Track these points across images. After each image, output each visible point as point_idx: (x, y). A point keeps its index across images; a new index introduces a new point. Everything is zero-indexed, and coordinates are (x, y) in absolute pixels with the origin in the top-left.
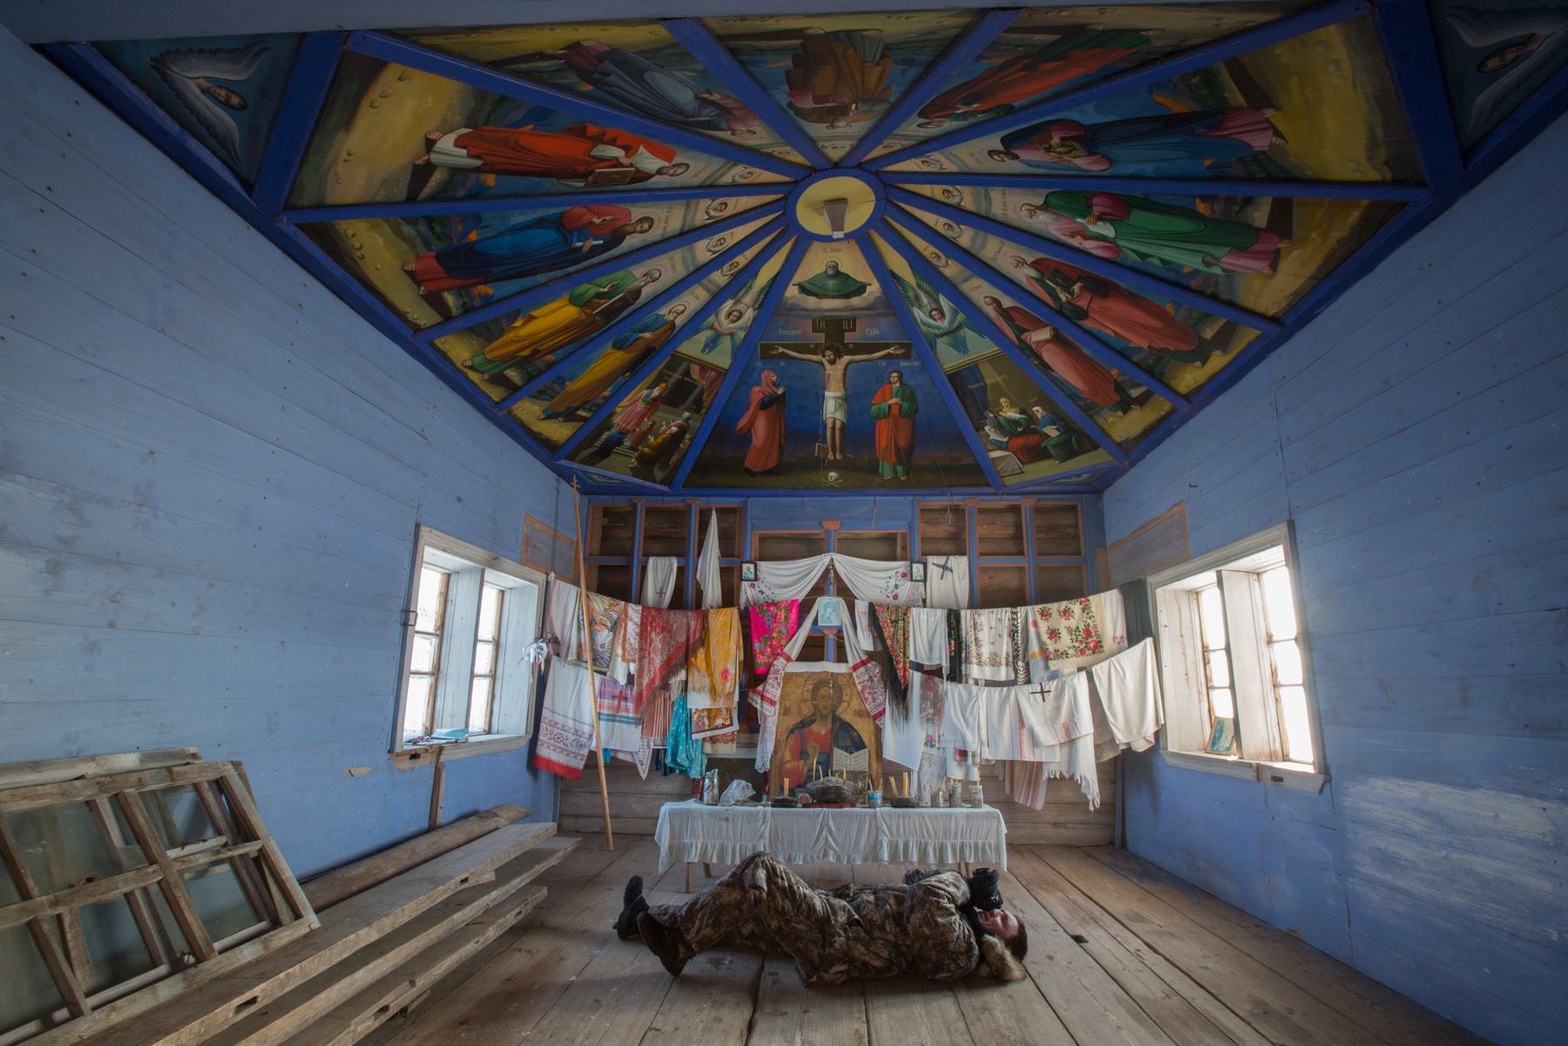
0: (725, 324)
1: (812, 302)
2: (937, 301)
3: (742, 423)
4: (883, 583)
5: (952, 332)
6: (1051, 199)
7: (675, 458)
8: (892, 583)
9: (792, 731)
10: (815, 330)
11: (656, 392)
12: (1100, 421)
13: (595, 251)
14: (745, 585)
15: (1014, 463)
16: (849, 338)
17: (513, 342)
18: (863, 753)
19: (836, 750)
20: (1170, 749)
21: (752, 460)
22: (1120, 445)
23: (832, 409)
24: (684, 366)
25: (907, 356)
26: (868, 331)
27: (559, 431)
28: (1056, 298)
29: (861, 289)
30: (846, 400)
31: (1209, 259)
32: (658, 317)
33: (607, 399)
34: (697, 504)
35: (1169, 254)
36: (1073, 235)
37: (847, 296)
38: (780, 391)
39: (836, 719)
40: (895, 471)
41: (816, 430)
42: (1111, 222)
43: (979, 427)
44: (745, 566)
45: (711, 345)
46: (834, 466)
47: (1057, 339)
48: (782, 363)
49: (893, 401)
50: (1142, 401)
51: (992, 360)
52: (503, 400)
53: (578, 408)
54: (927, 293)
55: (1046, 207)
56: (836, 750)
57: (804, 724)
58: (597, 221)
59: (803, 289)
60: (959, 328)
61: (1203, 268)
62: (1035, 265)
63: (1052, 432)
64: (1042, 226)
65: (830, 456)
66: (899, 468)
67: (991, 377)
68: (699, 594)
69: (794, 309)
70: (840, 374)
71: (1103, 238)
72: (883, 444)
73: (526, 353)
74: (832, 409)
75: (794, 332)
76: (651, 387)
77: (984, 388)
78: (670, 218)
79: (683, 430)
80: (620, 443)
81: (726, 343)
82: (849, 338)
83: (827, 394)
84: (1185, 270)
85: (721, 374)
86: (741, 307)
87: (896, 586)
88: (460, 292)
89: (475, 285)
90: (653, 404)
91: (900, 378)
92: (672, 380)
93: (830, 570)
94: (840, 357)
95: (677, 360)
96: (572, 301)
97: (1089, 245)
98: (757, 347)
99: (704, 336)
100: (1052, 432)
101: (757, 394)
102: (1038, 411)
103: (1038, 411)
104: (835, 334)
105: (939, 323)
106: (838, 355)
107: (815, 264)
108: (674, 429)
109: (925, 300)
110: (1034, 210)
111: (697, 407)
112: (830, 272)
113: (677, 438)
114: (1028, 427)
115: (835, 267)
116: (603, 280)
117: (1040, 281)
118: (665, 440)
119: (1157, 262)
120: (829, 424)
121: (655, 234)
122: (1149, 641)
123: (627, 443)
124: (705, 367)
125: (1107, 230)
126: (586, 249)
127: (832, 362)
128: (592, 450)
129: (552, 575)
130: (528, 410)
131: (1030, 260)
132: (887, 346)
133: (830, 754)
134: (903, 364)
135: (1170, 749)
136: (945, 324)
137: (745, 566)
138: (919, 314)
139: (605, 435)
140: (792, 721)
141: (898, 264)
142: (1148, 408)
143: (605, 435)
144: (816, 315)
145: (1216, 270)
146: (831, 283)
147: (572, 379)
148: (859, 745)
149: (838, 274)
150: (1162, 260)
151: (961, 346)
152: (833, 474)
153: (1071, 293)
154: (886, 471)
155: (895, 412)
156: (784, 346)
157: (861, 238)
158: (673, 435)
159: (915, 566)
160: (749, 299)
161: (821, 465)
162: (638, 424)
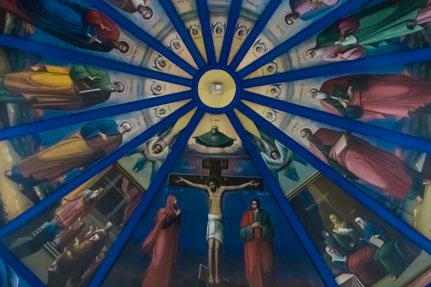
0: (151, 154)
1: (203, 149)
2: (274, 146)
3: (148, 241)
5: (286, 166)
6: (320, 39)
7: (88, 272)
10: (204, 167)
13: (95, 46)
16: (224, 173)
17: (25, 81)
24: (120, 176)
25: (261, 188)
26: (235, 169)
28: (339, 107)
29: (230, 142)
30: (225, 223)
31: (410, 23)
32: (115, 125)
35: (388, 34)
36: (336, 55)
37: (223, 146)
38: (178, 213)
42: (352, 34)
43: (321, 251)
45: (140, 166)
47: (353, 144)
48: (182, 190)
49: (255, 225)
51: (316, 181)
53: (37, 183)
54: (268, 142)
55: (318, 47)
58: (103, 28)
59: (198, 140)
60: (290, 161)
61: (410, 32)
62: (323, 90)
64: (319, 59)
65: (211, 280)
67: (320, 197)
69: (193, 152)
70: (218, 199)
71: (351, 47)
72: (251, 269)
73: (28, 96)
75: (191, 168)
76: (93, 188)
77: (316, 208)
78: (136, 54)
81: (148, 168)
82: (224, 173)
83: (211, 216)
84: (402, 39)
86: (162, 143)
88: (17, 20)
89: (27, 21)
90: (90, 203)
91: (258, 204)
92: (108, 187)
94: (219, 187)
95: (118, 170)
96: (73, 74)
97: (346, 56)
98: (167, 176)
99: (137, 157)
101: (162, 214)
104: (215, 165)
105: (277, 161)
106: (218, 185)
107: (206, 126)
109: (267, 146)
110: (312, 51)
112: (214, 132)
115: (216, 129)
116: (93, 70)
117: (328, 100)
119: (384, 44)
121: (127, 58)
124: (133, 184)
125: (351, 40)
126: (91, 41)
127: (214, 191)
128: (27, 239)
131: (319, 87)
132: (248, 180)
134: (260, 194)
136: (281, 161)
138: (265, 156)
141: (250, 126)
144: (205, 157)
145: (418, 28)
146: (214, 138)
149: (217, 133)
150: (388, 41)
151: (293, 175)
153: (347, 98)
155: (257, 235)
156: (184, 177)
157: (228, 111)
158: (95, 243)
160: (167, 139)
162: (71, 223)
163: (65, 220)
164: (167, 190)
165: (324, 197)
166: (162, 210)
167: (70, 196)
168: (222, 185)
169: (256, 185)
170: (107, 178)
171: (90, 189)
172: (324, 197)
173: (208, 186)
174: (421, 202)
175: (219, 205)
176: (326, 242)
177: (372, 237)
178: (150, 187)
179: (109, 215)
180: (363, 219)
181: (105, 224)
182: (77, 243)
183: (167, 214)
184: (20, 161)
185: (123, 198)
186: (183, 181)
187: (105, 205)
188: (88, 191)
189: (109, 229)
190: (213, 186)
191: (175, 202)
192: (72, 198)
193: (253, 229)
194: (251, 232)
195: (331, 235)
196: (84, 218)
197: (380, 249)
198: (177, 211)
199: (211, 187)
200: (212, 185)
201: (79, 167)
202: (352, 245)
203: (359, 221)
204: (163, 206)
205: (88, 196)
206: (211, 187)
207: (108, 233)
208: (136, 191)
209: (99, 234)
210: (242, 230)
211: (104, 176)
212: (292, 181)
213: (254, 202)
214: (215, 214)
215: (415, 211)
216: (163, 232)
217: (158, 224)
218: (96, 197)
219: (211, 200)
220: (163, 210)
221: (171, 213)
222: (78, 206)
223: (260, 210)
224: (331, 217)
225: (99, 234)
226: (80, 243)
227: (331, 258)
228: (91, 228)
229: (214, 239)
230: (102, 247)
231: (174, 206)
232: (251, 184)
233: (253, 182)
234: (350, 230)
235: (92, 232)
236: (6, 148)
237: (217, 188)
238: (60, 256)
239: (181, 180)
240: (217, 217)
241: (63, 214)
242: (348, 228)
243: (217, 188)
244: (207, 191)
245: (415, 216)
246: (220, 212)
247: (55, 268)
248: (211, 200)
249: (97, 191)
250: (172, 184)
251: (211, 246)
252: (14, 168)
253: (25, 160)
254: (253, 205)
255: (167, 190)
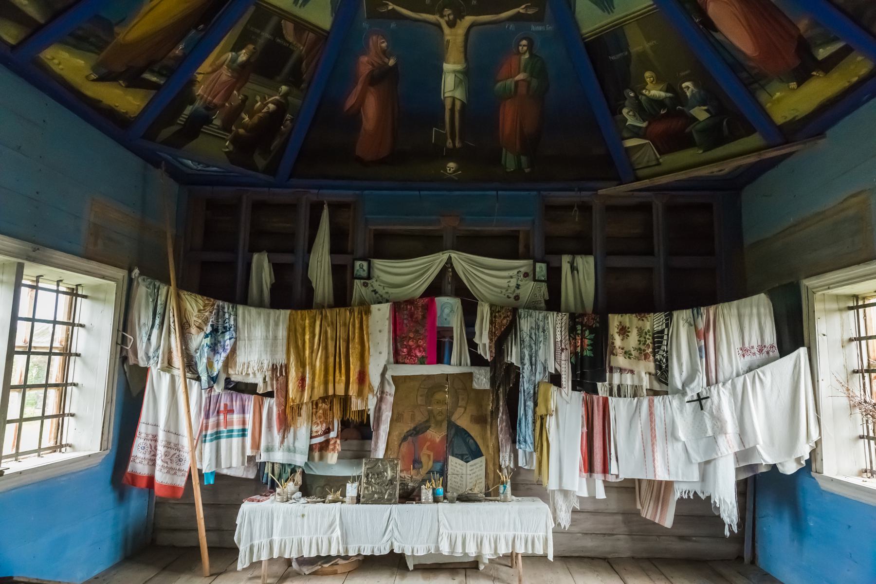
3: (351, 101)
4: (503, 283)
7: (276, 143)
8: (513, 282)
9: (405, 439)
11: (243, 56)
12: (763, 97)
14: (358, 283)
15: (651, 153)
18: (480, 462)
19: (451, 458)
20: (826, 473)
21: (364, 148)
22: (780, 128)
23: (451, 86)
24: (274, 21)
27: (127, 101)
30: (467, 76)
33: (181, 60)
34: (313, 195)
38: (392, 62)
39: (451, 425)
40: (519, 162)
41: (432, 108)
43: (615, 111)
44: (358, 264)
46: (452, 155)
49: (520, 77)
50: (828, 66)
52: (21, 43)
53: (143, 70)
56: (451, 458)
57: (417, 431)
63: (701, 114)
65: (449, 143)
66: (523, 159)
67: (639, 43)
68: (310, 290)
70: (460, 39)
74: (451, 86)
76: (237, 48)
77: (627, 59)
79: (282, 108)
80: (208, 121)
83: (447, 67)
85: (322, 36)
87: (518, 287)
90: (242, 72)
91: (530, 46)
92: (261, 41)
93: (447, 274)
94: (462, 17)
100: (701, 114)
101: (365, 65)
102: (688, 87)
103: (688, 87)
108: (271, 106)
111: (295, 79)
113: (276, 118)
114: (675, 106)
118: (261, 120)
120: (448, 104)
122: (802, 351)
123: (217, 122)
124: (301, 26)
127: (452, 24)
128: (174, 128)
129: (136, 272)
130: (67, 62)
133: (446, 461)
134: (535, 28)
135: (826, 473)
137: (358, 264)
139: (189, 110)
140: (406, 427)
142: (835, 75)
143: (189, 110)
147: (122, 21)
148: (476, 453)
152: (452, 165)
154: (510, 162)
155: (522, 90)
158: (271, 114)
159: (538, 265)
161: (440, 154)
162: (228, 96)
163: (214, 97)
164: (365, 25)
165: (647, 46)
166: (364, 59)
167: (206, 66)
168: (468, 15)
169: (530, 12)
170: (252, 29)
171: (232, 51)
172: (647, 46)
173: (442, 16)
174: (793, 89)
175: (462, 49)
176: (627, 103)
177: (696, 108)
178: (333, 25)
179: (278, 78)
180: (695, 85)
181: (277, 90)
182: (247, 119)
183: (373, 65)
184: (94, 58)
185: (292, 52)
186: (393, 9)
187: (269, 63)
188: (230, 55)
189: (285, 95)
190: (451, 17)
191: (384, 45)
192: (210, 70)
193: (517, 82)
194: (513, 87)
195: (636, 97)
196: (243, 89)
197: (700, 122)
198: (389, 59)
199: (446, 18)
200: (449, 15)
201: (196, 27)
202: (662, 112)
203: (688, 87)
204: (365, 52)
205: (233, 60)
206: (446, 18)
207: (287, 100)
208: (311, 35)
209: (272, 102)
210: (499, 84)
211: (246, 25)
212: (600, 12)
213: (524, 42)
214: (454, 63)
215: (778, 94)
216: (372, 89)
217: (361, 79)
218: (248, 60)
219: (448, 41)
220: (366, 59)
221: (380, 62)
222: (224, 78)
223: (531, 55)
224: (648, 74)
225: (272, 102)
226: (250, 118)
227: (626, 120)
228: (258, 98)
229: (454, 99)
230: (284, 116)
231: (384, 52)
232: (521, 11)
233: (526, 8)
234: (669, 95)
235: (262, 103)
236: (61, 52)
237: (458, 21)
238: (230, 136)
239: (390, 8)
240: (459, 67)
241: (208, 91)
242: (667, 91)
243: (458, 21)
244: (438, 26)
245: (774, 98)
246: (463, 60)
247: (231, 148)
248: (448, 41)
249: (244, 51)
250: (374, 15)
251: (448, 106)
252: (94, 69)
253: (103, 54)
254: (520, 48)
255: (365, 25)
